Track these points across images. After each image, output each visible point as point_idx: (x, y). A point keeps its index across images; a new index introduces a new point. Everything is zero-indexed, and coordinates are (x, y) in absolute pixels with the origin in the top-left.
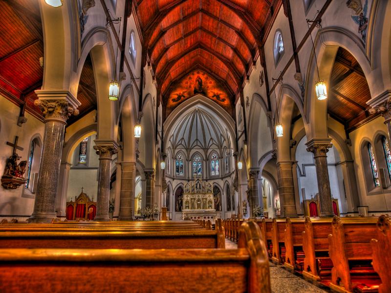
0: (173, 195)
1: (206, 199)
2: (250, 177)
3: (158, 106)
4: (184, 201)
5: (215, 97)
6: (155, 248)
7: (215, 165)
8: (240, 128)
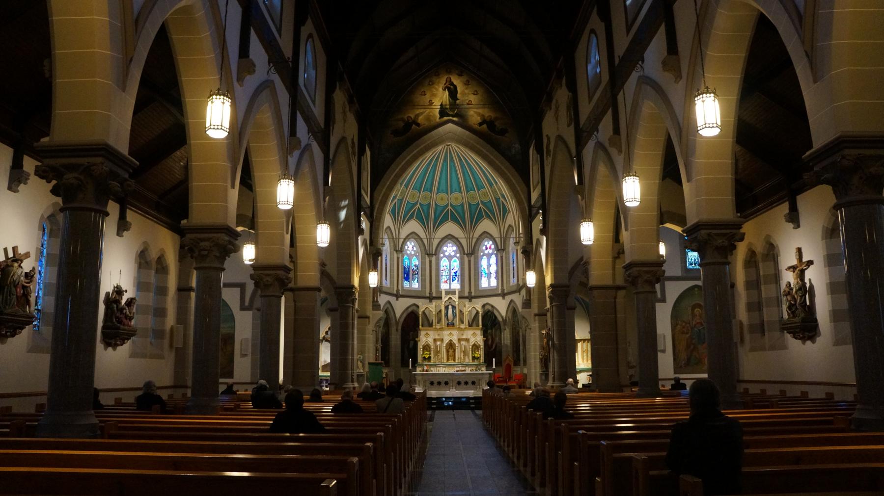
0: (397, 330)
1: (467, 340)
2: (551, 303)
3: (362, 152)
4: (420, 345)
5: (485, 126)
6: (353, 328)
7: (489, 265)
8: (535, 196)
